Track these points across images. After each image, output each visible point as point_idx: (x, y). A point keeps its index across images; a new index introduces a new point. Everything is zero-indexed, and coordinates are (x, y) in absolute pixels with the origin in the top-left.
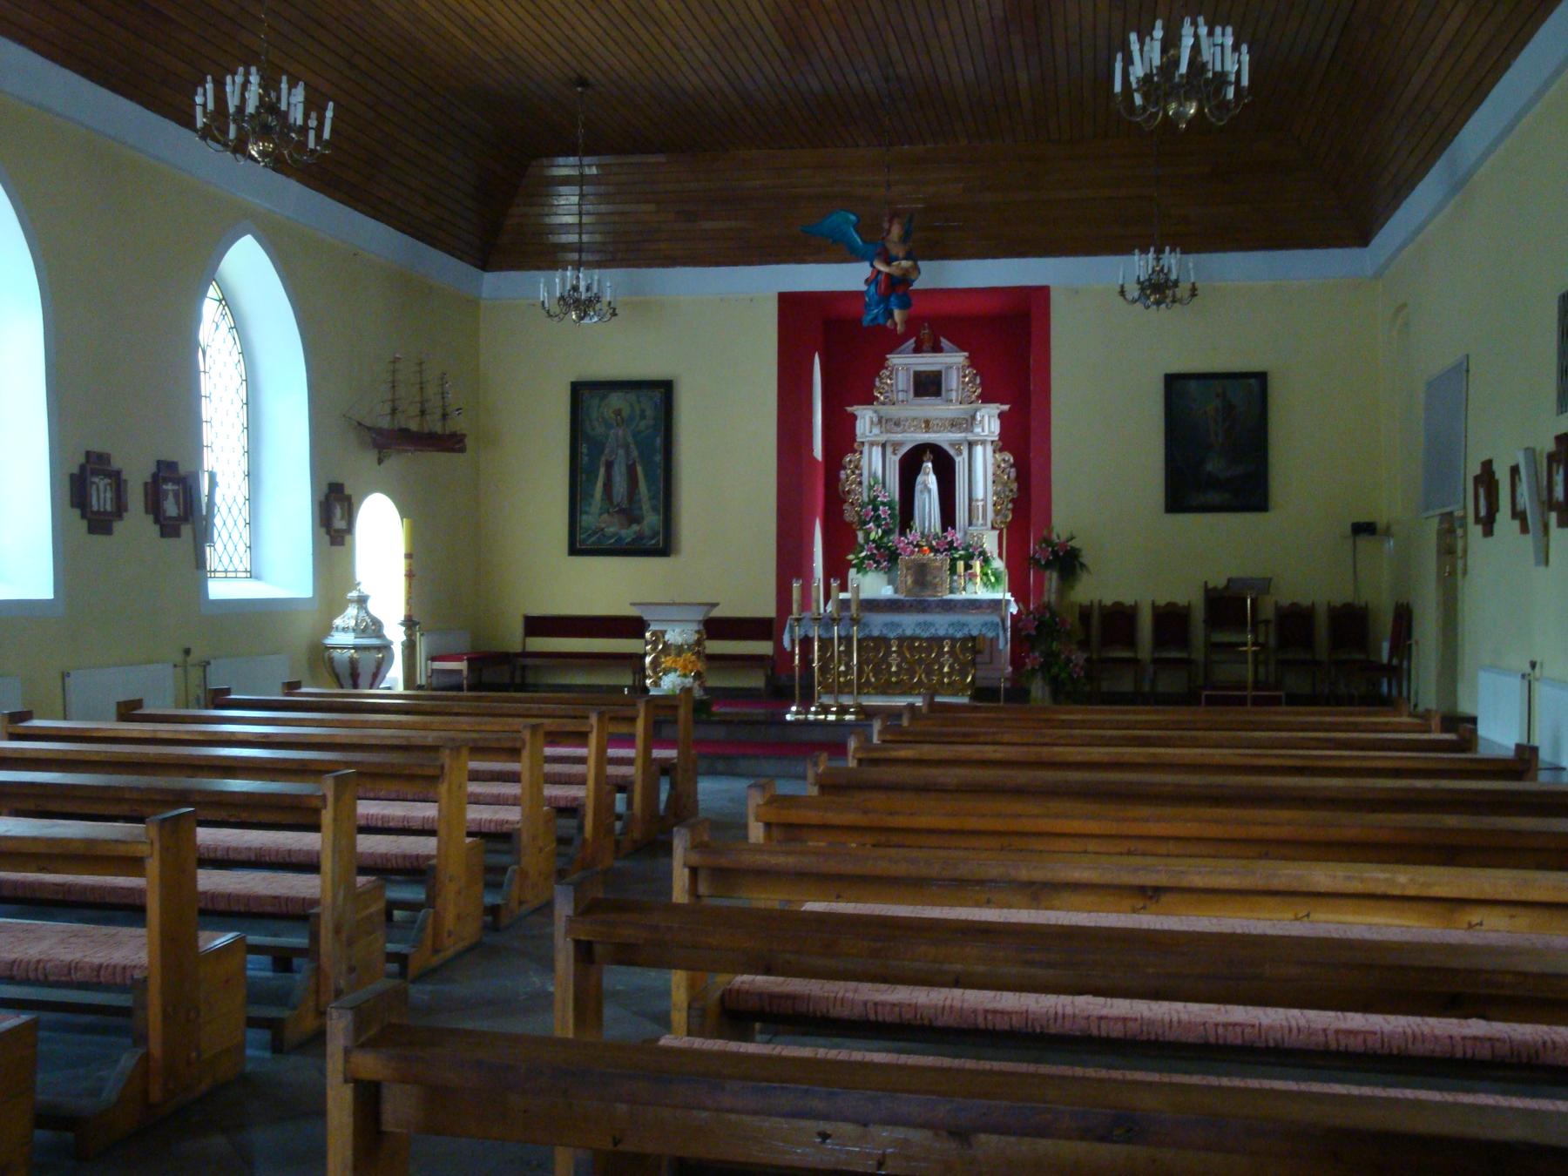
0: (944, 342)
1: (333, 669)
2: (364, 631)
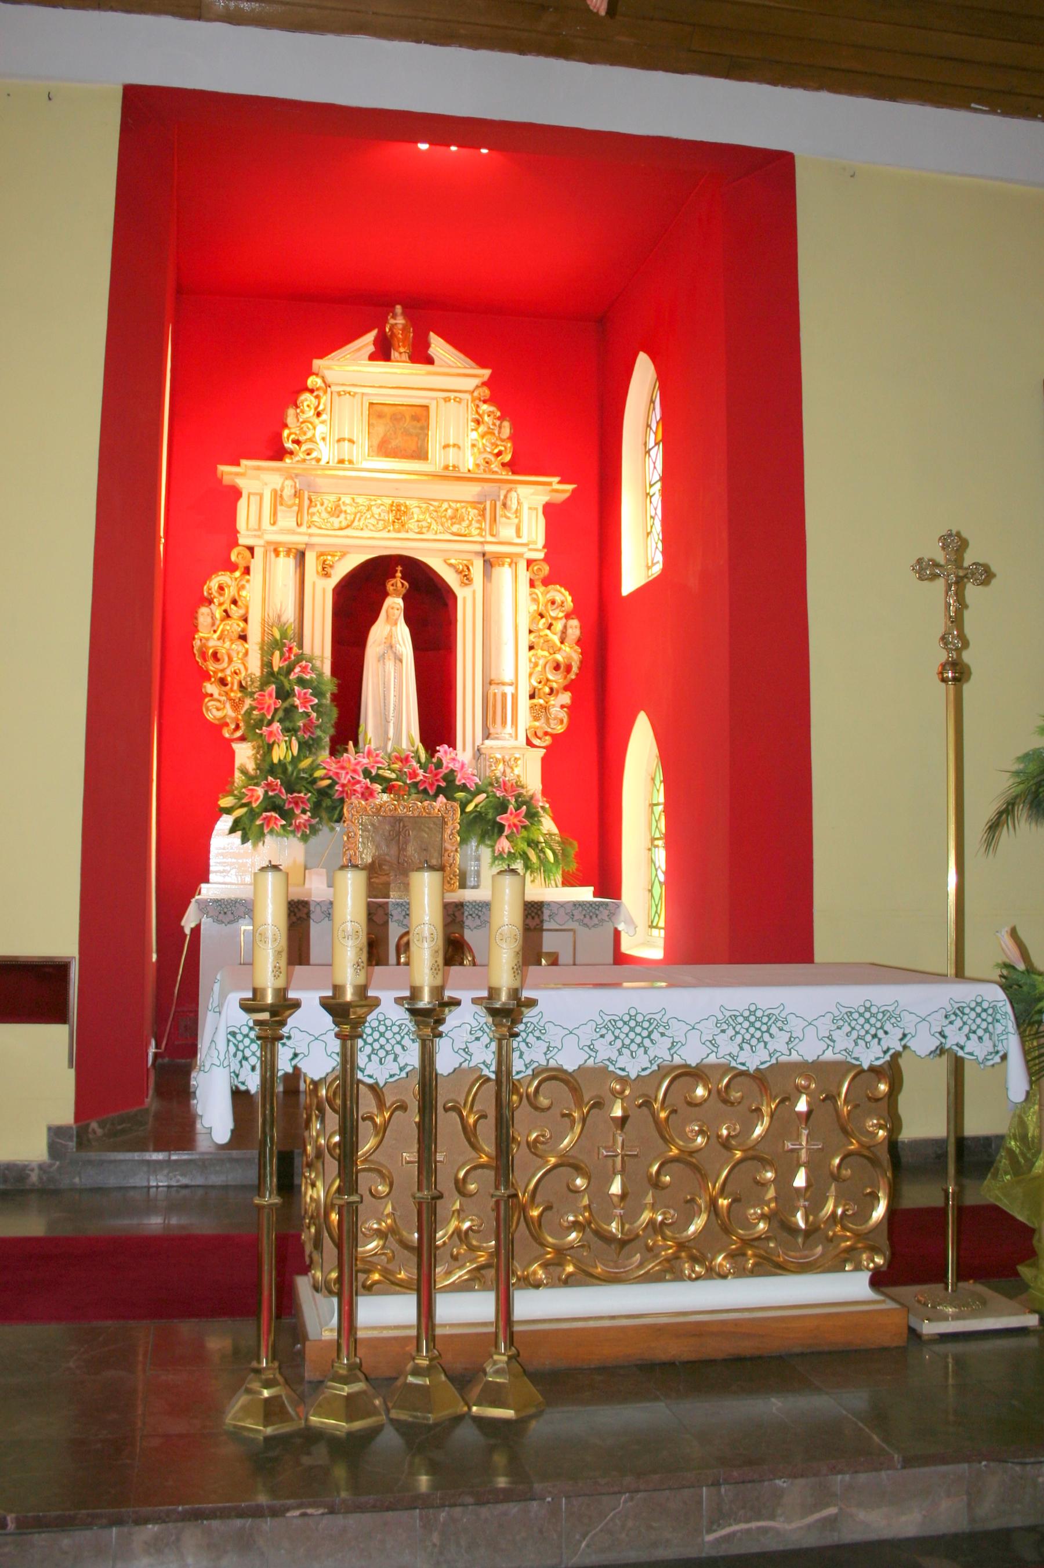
0: (438, 346)
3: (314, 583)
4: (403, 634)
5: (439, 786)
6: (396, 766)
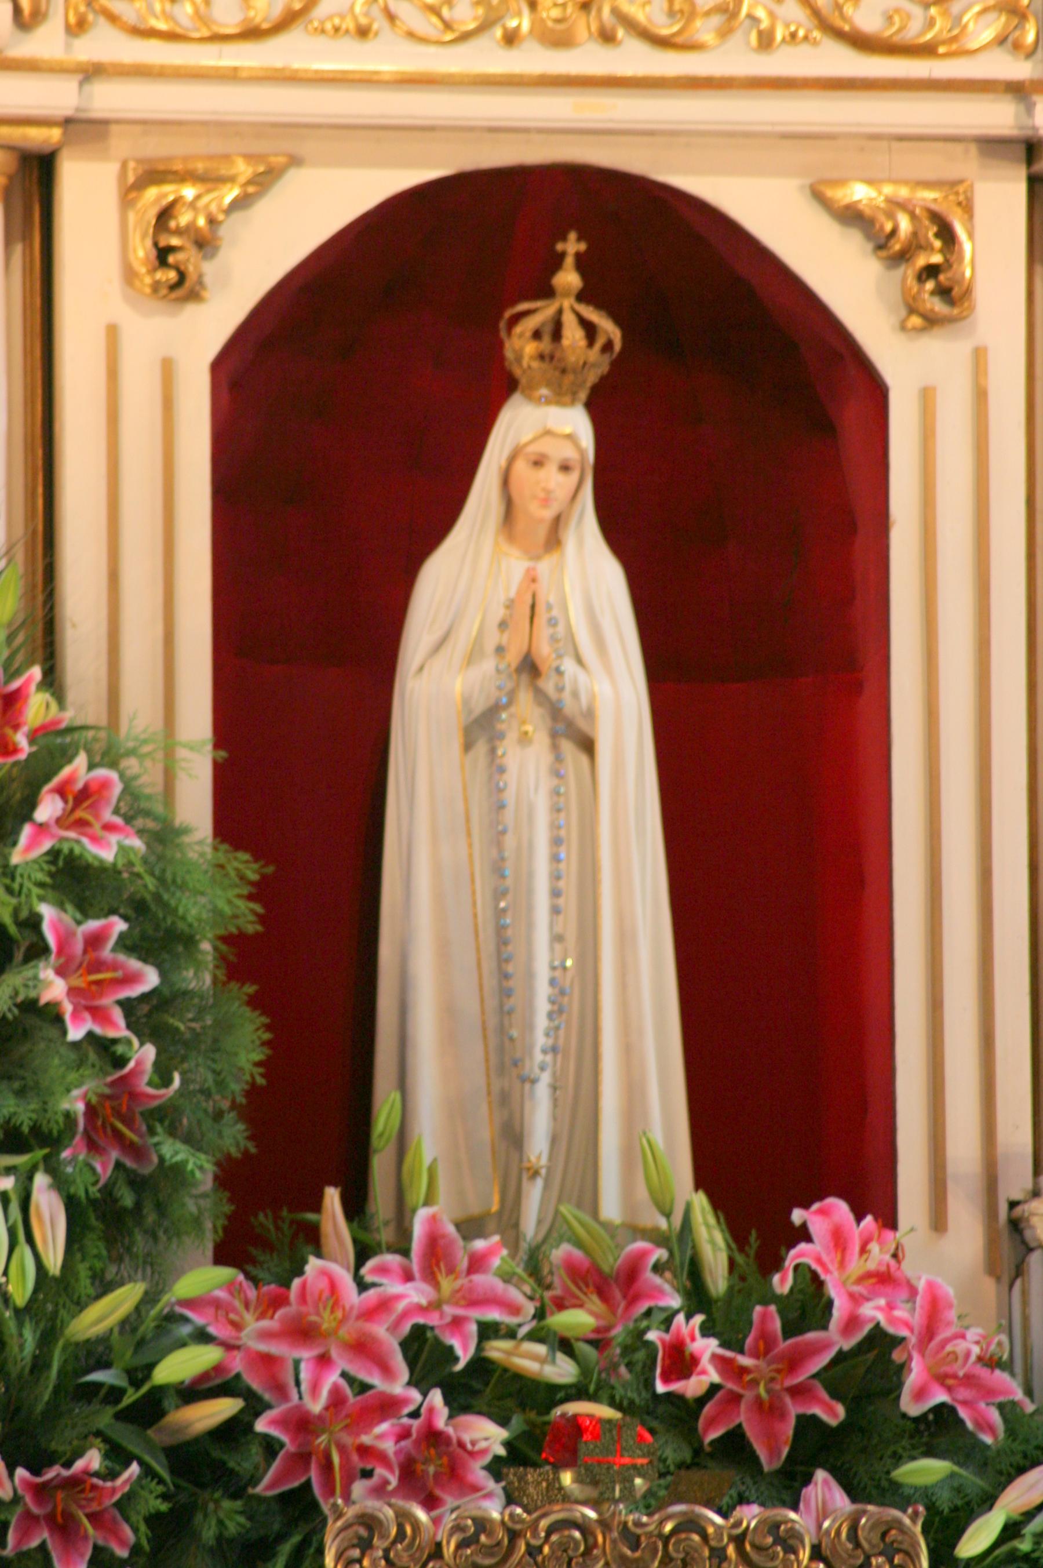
3: (112, 333)
4: (592, 587)
5: (807, 1424)
6: (577, 1320)
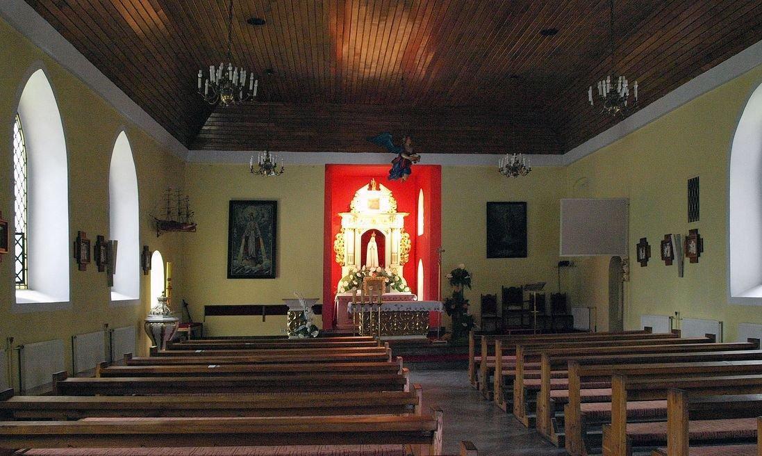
1: (151, 331)
2: (167, 315)
